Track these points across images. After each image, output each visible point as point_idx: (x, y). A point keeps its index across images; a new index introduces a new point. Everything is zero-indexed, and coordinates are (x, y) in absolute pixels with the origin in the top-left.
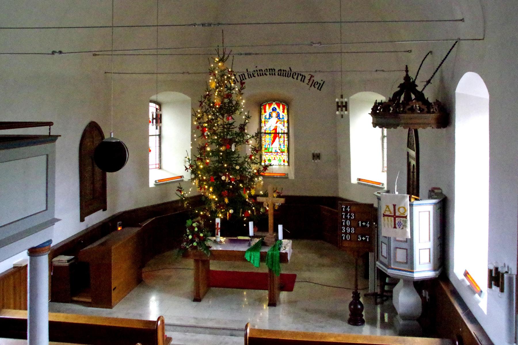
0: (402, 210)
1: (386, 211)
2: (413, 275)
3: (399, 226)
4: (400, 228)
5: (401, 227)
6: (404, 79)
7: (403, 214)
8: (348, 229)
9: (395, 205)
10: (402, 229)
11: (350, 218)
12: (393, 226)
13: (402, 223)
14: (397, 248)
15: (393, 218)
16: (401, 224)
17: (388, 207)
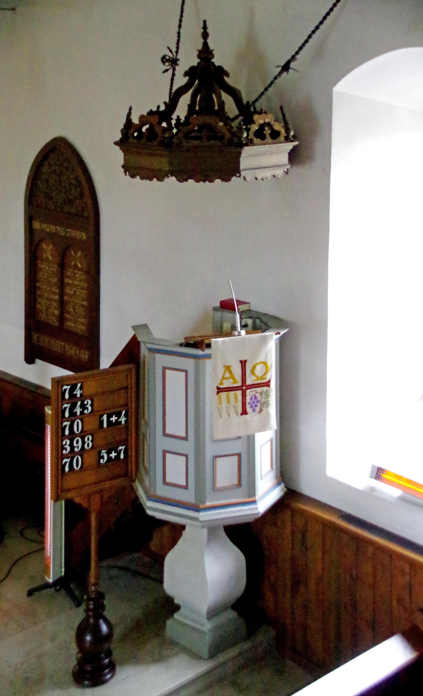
0: (259, 371)
1: (224, 378)
2: (257, 508)
3: (251, 407)
4: (254, 410)
5: (258, 409)
6: (199, 57)
7: (262, 378)
8: (77, 442)
9: (246, 361)
10: (259, 412)
11: (82, 413)
12: (240, 411)
13: (259, 398)
14: (217, 457)
15: (239, 393)
16: (258, 402)
17: (228, 368)
